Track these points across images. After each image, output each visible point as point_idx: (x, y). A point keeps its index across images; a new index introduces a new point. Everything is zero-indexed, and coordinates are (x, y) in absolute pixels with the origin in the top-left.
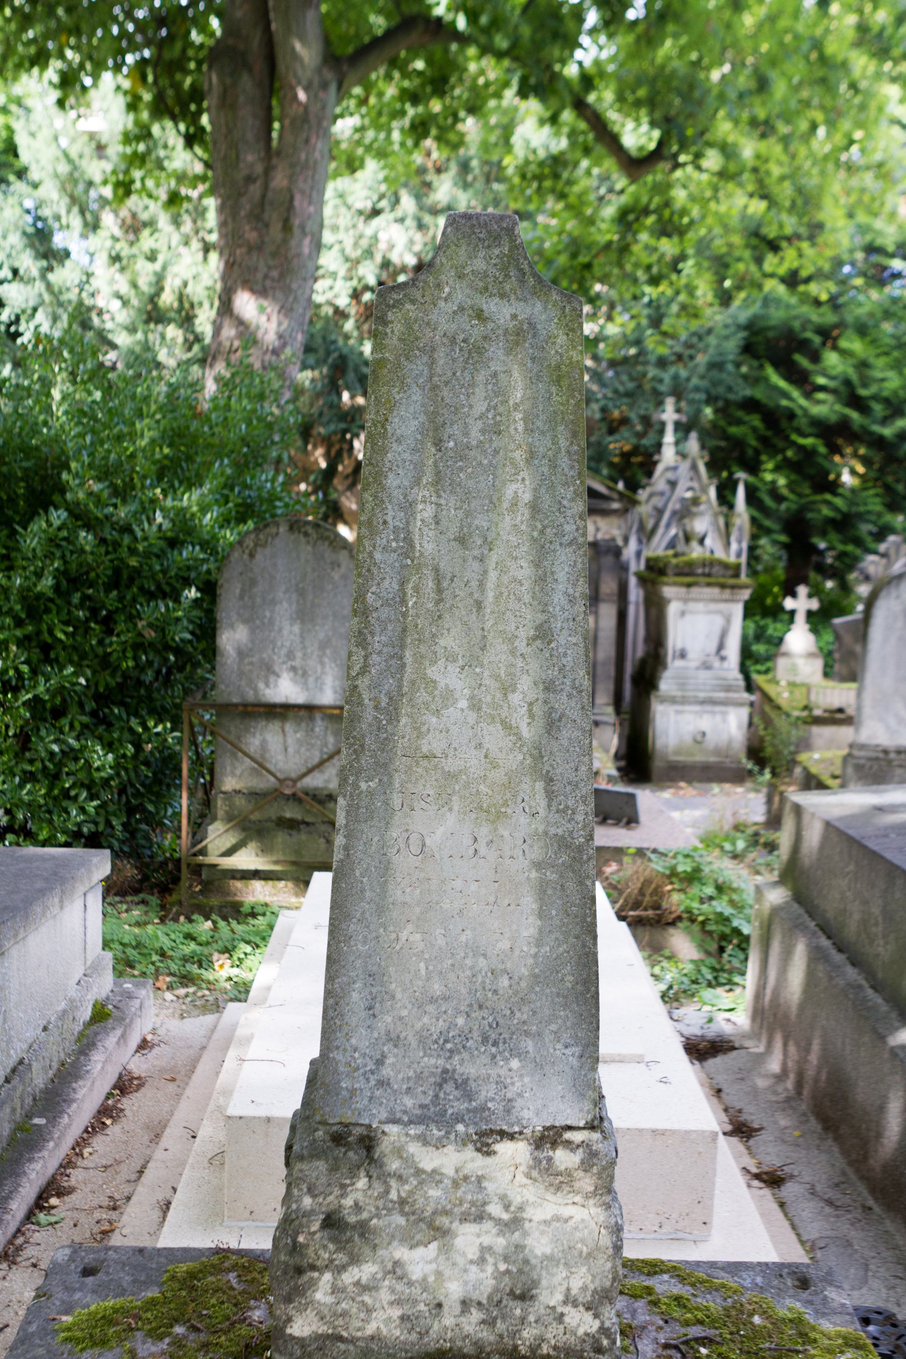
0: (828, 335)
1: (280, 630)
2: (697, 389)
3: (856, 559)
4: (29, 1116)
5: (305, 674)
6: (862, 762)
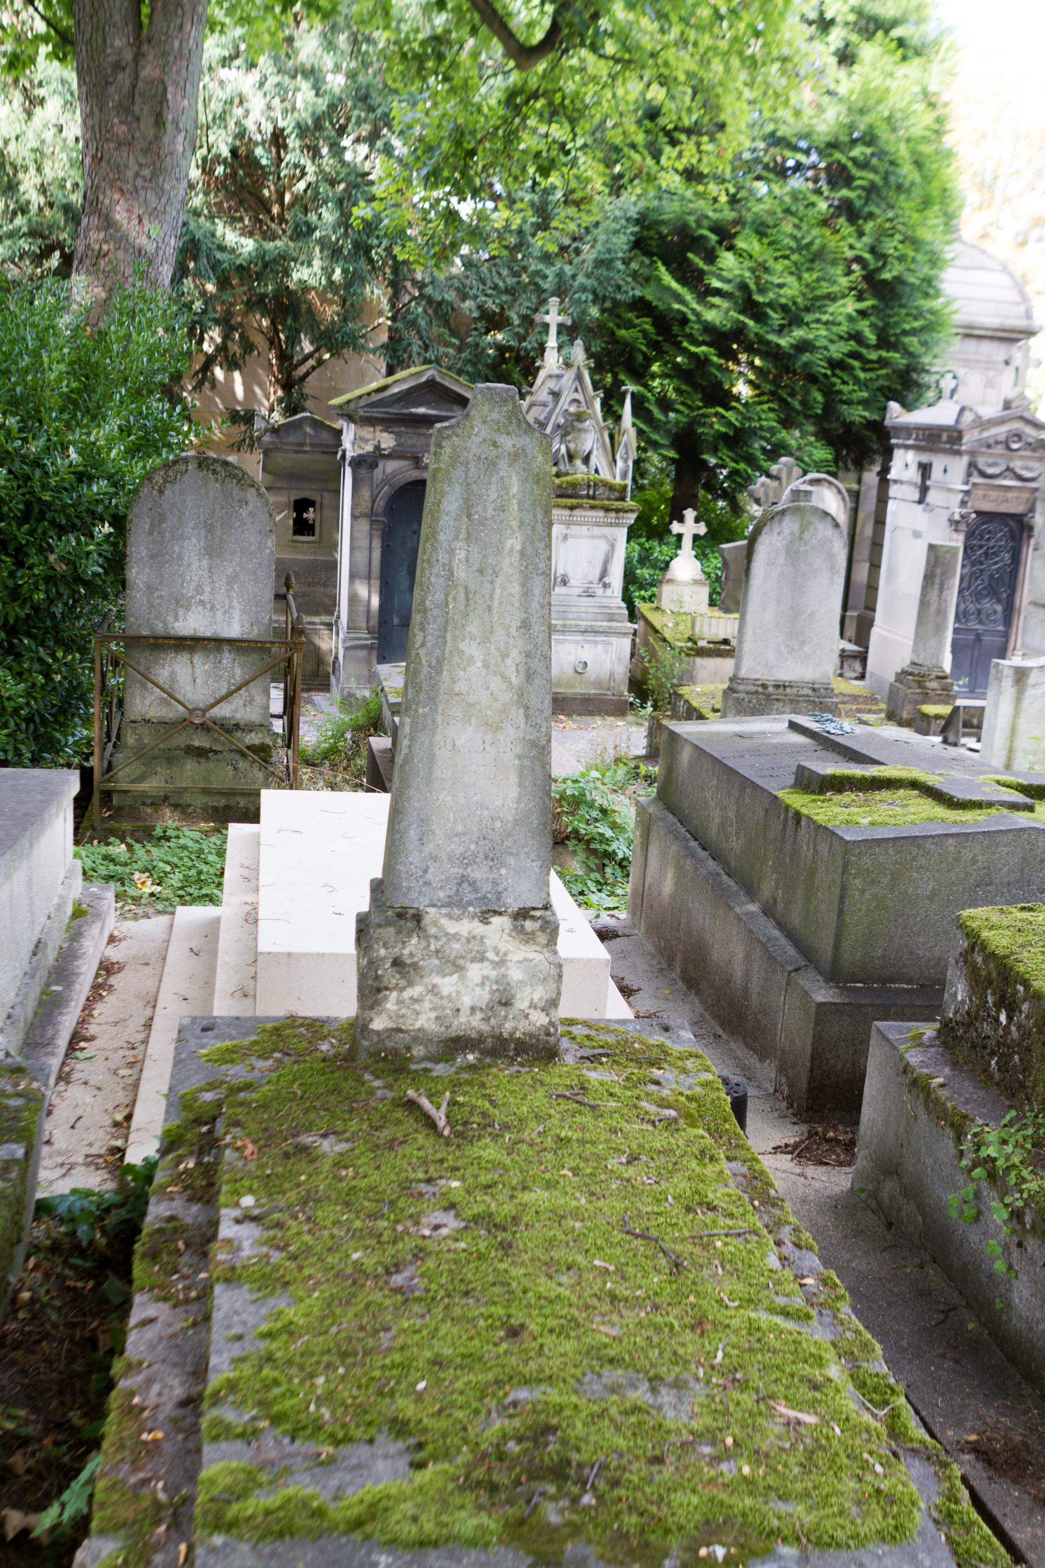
0: (725, 235)
1: (189, 565)
2: (583, 289)
3: (749, 479)
4: (48, 985)
5: (213, 608)
6: (742, 695)
